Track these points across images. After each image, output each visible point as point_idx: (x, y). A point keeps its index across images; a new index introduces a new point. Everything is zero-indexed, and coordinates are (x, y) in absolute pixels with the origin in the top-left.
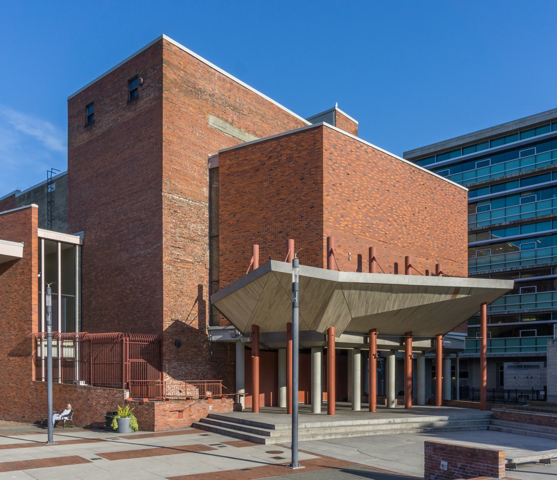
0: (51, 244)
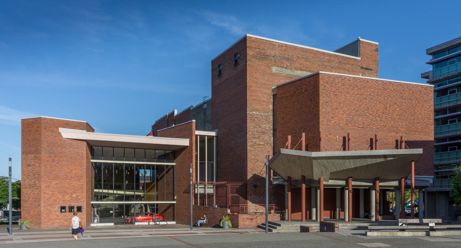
0: (202, 137)
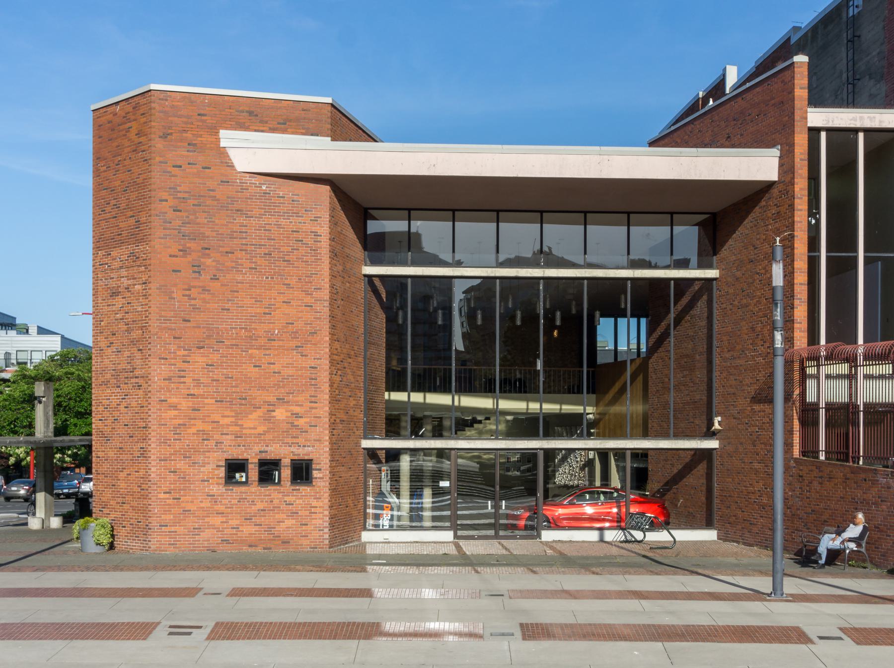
0: (842, 137)
